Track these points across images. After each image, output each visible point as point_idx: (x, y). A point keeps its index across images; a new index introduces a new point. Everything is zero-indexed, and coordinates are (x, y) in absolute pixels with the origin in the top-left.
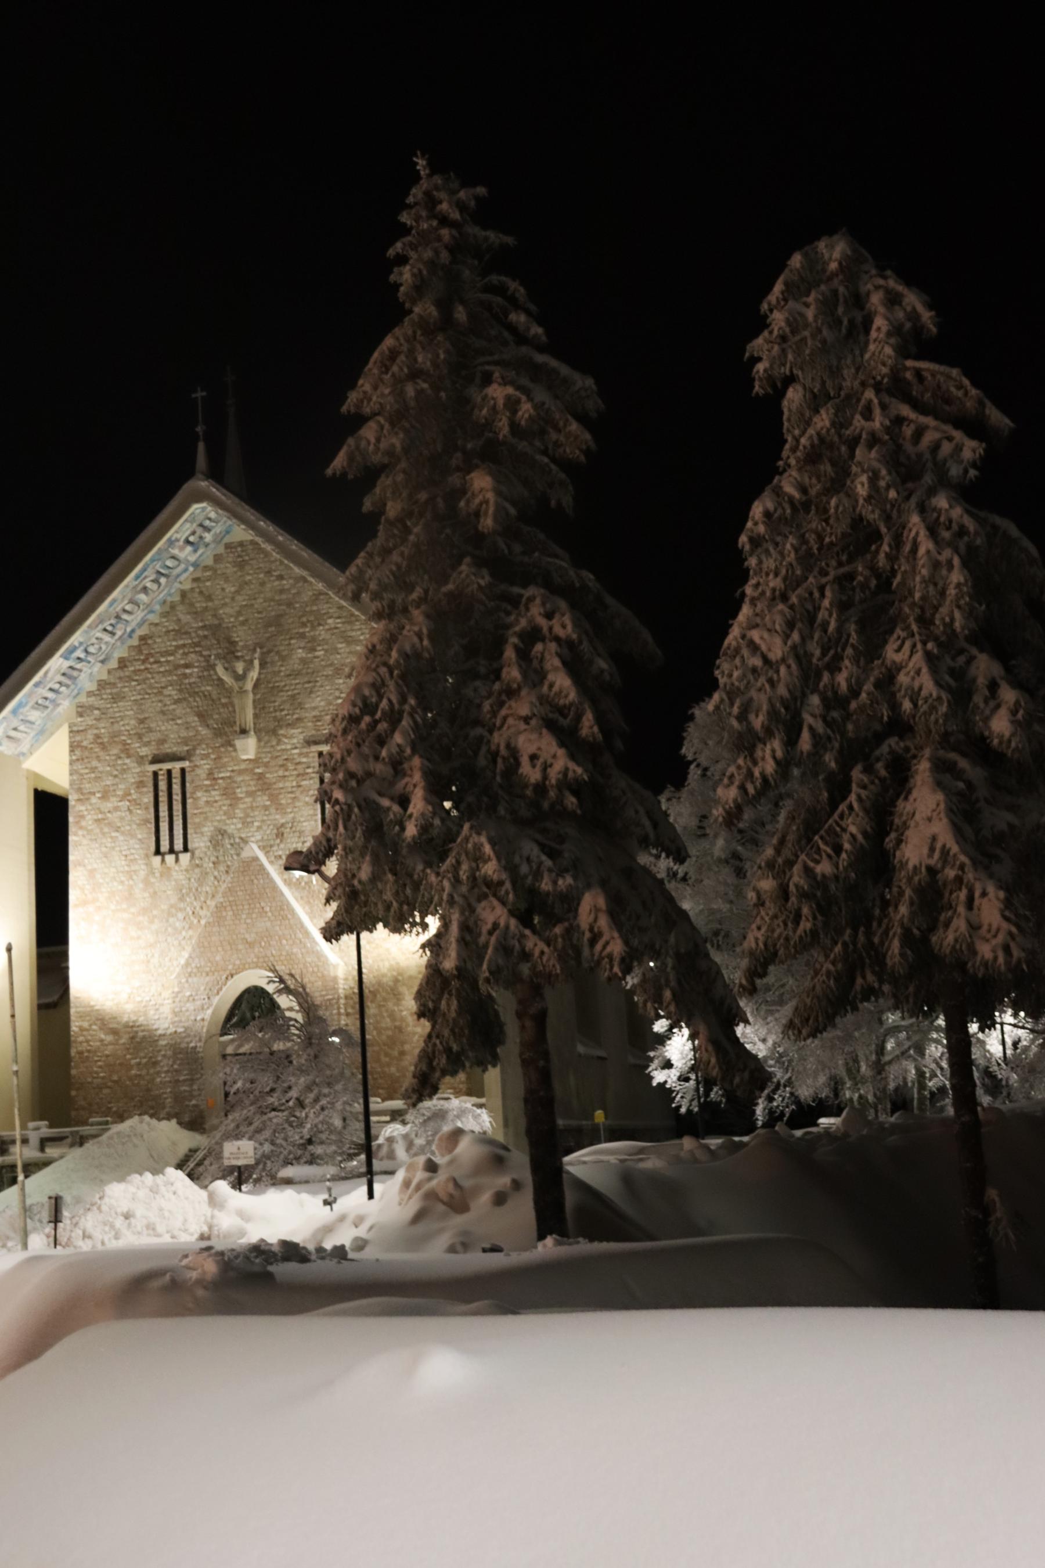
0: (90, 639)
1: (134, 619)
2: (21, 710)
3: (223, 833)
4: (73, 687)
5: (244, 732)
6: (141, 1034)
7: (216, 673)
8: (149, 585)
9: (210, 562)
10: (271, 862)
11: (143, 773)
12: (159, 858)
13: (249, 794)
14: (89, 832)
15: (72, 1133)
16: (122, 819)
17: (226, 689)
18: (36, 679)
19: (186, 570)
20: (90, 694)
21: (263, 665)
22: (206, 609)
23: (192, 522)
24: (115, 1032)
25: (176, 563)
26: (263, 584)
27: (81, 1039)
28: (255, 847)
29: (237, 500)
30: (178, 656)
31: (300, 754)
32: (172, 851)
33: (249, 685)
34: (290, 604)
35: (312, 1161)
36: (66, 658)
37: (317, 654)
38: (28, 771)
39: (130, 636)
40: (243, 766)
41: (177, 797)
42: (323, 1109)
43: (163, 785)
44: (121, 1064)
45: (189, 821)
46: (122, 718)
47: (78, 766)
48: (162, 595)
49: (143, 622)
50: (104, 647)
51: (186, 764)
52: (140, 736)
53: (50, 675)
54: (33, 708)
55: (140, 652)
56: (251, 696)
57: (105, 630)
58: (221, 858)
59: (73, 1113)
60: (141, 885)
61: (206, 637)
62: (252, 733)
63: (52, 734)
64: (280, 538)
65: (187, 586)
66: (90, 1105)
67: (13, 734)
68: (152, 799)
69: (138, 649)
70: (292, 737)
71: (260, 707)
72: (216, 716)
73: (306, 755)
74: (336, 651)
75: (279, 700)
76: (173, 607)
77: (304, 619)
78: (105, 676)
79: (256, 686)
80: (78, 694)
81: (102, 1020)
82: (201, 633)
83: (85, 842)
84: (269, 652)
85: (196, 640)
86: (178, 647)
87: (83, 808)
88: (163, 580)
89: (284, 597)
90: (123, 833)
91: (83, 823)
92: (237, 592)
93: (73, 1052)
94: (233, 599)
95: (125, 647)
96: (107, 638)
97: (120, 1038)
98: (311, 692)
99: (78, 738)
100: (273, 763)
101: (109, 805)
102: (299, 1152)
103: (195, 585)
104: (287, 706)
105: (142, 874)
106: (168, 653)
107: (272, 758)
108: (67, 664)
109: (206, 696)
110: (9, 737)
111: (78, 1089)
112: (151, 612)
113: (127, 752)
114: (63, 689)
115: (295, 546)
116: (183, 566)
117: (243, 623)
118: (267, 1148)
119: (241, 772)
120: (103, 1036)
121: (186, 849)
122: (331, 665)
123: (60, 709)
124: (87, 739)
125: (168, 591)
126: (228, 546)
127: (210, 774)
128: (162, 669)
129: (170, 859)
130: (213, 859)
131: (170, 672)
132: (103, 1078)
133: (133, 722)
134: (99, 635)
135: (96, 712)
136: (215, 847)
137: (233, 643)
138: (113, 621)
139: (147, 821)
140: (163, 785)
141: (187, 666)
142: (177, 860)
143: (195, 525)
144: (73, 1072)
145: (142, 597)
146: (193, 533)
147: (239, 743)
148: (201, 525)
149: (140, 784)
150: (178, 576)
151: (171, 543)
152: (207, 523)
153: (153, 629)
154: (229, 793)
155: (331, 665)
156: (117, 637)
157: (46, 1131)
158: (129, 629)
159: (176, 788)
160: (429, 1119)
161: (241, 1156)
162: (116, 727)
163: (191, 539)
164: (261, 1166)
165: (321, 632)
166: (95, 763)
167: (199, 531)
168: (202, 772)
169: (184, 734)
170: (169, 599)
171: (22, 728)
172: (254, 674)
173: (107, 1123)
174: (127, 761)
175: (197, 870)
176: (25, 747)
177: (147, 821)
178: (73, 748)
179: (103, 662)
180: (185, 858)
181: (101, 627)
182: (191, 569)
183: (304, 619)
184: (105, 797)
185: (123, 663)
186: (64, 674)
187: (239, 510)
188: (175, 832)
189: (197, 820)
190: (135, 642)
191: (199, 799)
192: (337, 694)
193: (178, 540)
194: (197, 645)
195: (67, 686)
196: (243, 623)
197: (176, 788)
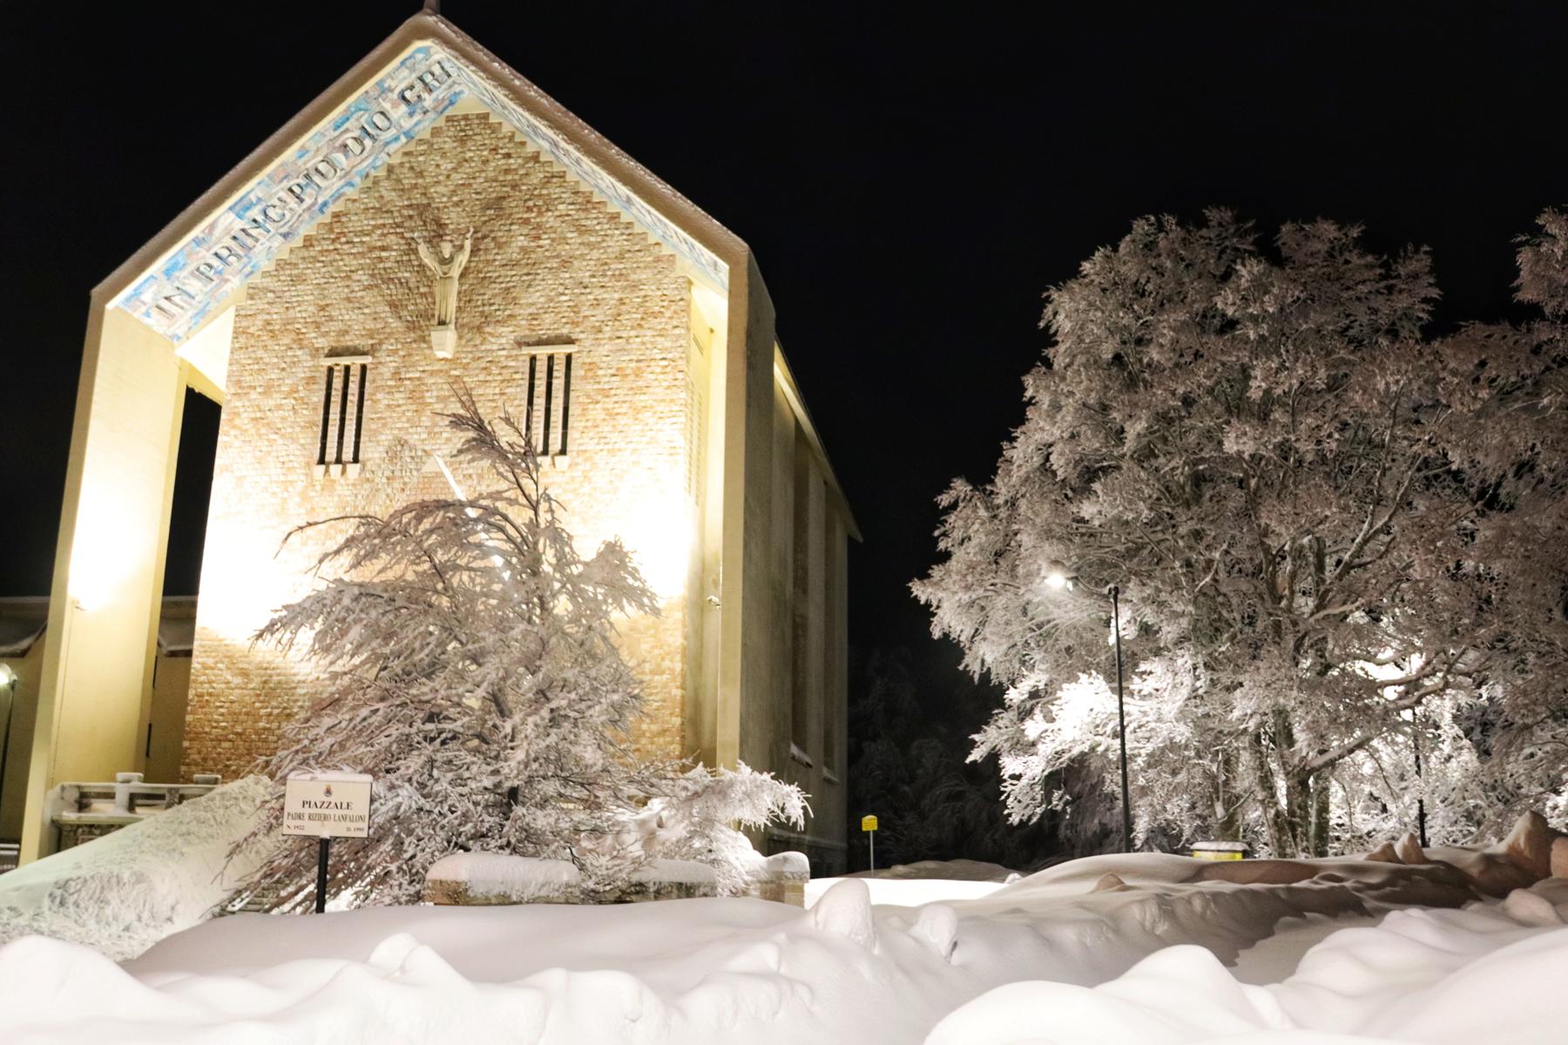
0: (271, 196)
1: (332, 185)
2: (177, 273)
3: (402, 443)
4: (245, 260)
5: (442, 323)
6: (275, 679)
7: (419, 258)
8: (350, 143)
9: (427, 136)
10: (459, 482)
11: (316, 368)
12: (323, 467)
13: (440, 399)
14: (244, 432)
15: (170, 790)
16: (284, 419)
17: (428, 278)
18: (196, 232)
19: (397, 139)
20: (266, 274)
21: (474, 251)
22: (415, 186)
23: (412, 69)
24: (245, 674)
25: (386, 123)
26: (485, 162)
27: (203, 678)
28: (440, 461)
29: (469, 39)
30: (375, 237)
31: (507, 357)
32: (339, 461)
33: (456, 272)
34: (514, 187)
35: (528, 844)
36: (240, 216)
37: (541, 242)
38: (182, 360)
39: (321, 211)
40: (437, 367)
41: (353, 398)
42: (555, 721)
43: (338, 383)
44: (247, 714)
45: (364, 426)
46: (299, 303)
47: (241, 355)
48: (365, 164)
49: (337, 197)
50: (288, 216)
51: (367, 360)
52: (318, 325)
53: (217, 232)
54: (192, 274)
55: (331, 230)
56: (456, 283)
57: (291, 190)
58: (397, 473)
59: (183, 768)
60: (297, 499)
61: (411, 217)
62: (452, 326)
63: (216, 317)
64: (517, 82)
65: (396, 160)
66: (205, 760)
67: (165, 304)
68: (323, 399)
69: (330, 227)
70: (500, 336)
71: (466, 299)
72: (411, 308)
73: (516, 358)
74: (564, 240)
75: (489, 293)
76: (376, 182)
77: (531, 203)
78: (286, 256)
79: (462, 276)
80: (251, 273)
81: (231, 659)
82: (405, 212)
83: (237, 443)
84: (484, 237)
85: (398, 220)
86: (376, 227)
87: (239, 404)
88: (368, 142)
89: (509, 177)
90: (283, 436)
91: (237, 422)
92: (454, 169)
93: (191, 694)
94: (448, 176)
95: (314, 223)
96: (292, 202)
97: (251, 681)
98: (529, 286)
99: (244, 324)
100: (474, 365)
101: (271, 402)
102: (490, 821)
103: (406, 159)
104: (498, 300)
105: (300, 486)
106: (363, 233)
107: (474, 359)
108: (240, 224)
109: (403, 283)
110: (158, 307)
111: (191, 740)
112: (350, 184)
113: (299, 341)
114: (232, 259)
115: (534, 92)
116: (393, 131)
117: (456, 204)
118: (407, 797)
119: (432, 373)
120: (229, 678)
121: (356, 460)
122: (557, 256)
123: (227, 287)
124: (255, 326)
125: (374, 160)
126: (449, 119)
127: (396, 375)
128: (354, 251)
129: (335, 469)
130: (388, 473)
131: (362, 254)
132: (224, 728)
133: (311, 309)
134: (283, 195)
135: (270, 295)
136: (391, 460)
137: (441, 226)
138: (302, 181)
139: (314, 424)
140: (338, 383)
141: (383, 249)
142: (344, 472)
143: (414, 76)
144: (189, 718)
145: (339, 157)
146: (411, 88)
147: (436, 335)
148: (421, 79)
149: (311, 380)
150: (387, 144)
151: (384, 91)
152: (428, 78)
153: (350, 205)
154: (416, 397)
155: (557, 256)
156: (305, 205)
157: (138, 785)
158: (320, 200)
159: (354, 387)
160: (696, 794)
161: (332, 812)
162: (291, 313)
163: (408, 94)
164: (386, 847)
165: (549, 219)
166: (260, 353)
167: (419, 86)
168: (386, 371)
169: (370, 325)
170: (373, 173)
171: (176, 299)
172: (463, 258)
173: (216, 781)
174: (299, 353)
175: (367, 486)
176: (180, 327)
177: (314, 424)
178: (237, 333)
179: (285, 236)
180: (353, 469)
181: (286, 184)
182: (403, 139)
183: (531, 203)
184: (268, 391)
185: (309, 242)
186: (235, 238)
187: (470, 49)
188: (346, 439)
189: (374, 426)
190: (326, 218)
191: (378, 402)
192: (561, 289)
193: (391, 90)
194: (398, 226)
195: (239, 257)
196: (456, 204)
197: (354, 387)
